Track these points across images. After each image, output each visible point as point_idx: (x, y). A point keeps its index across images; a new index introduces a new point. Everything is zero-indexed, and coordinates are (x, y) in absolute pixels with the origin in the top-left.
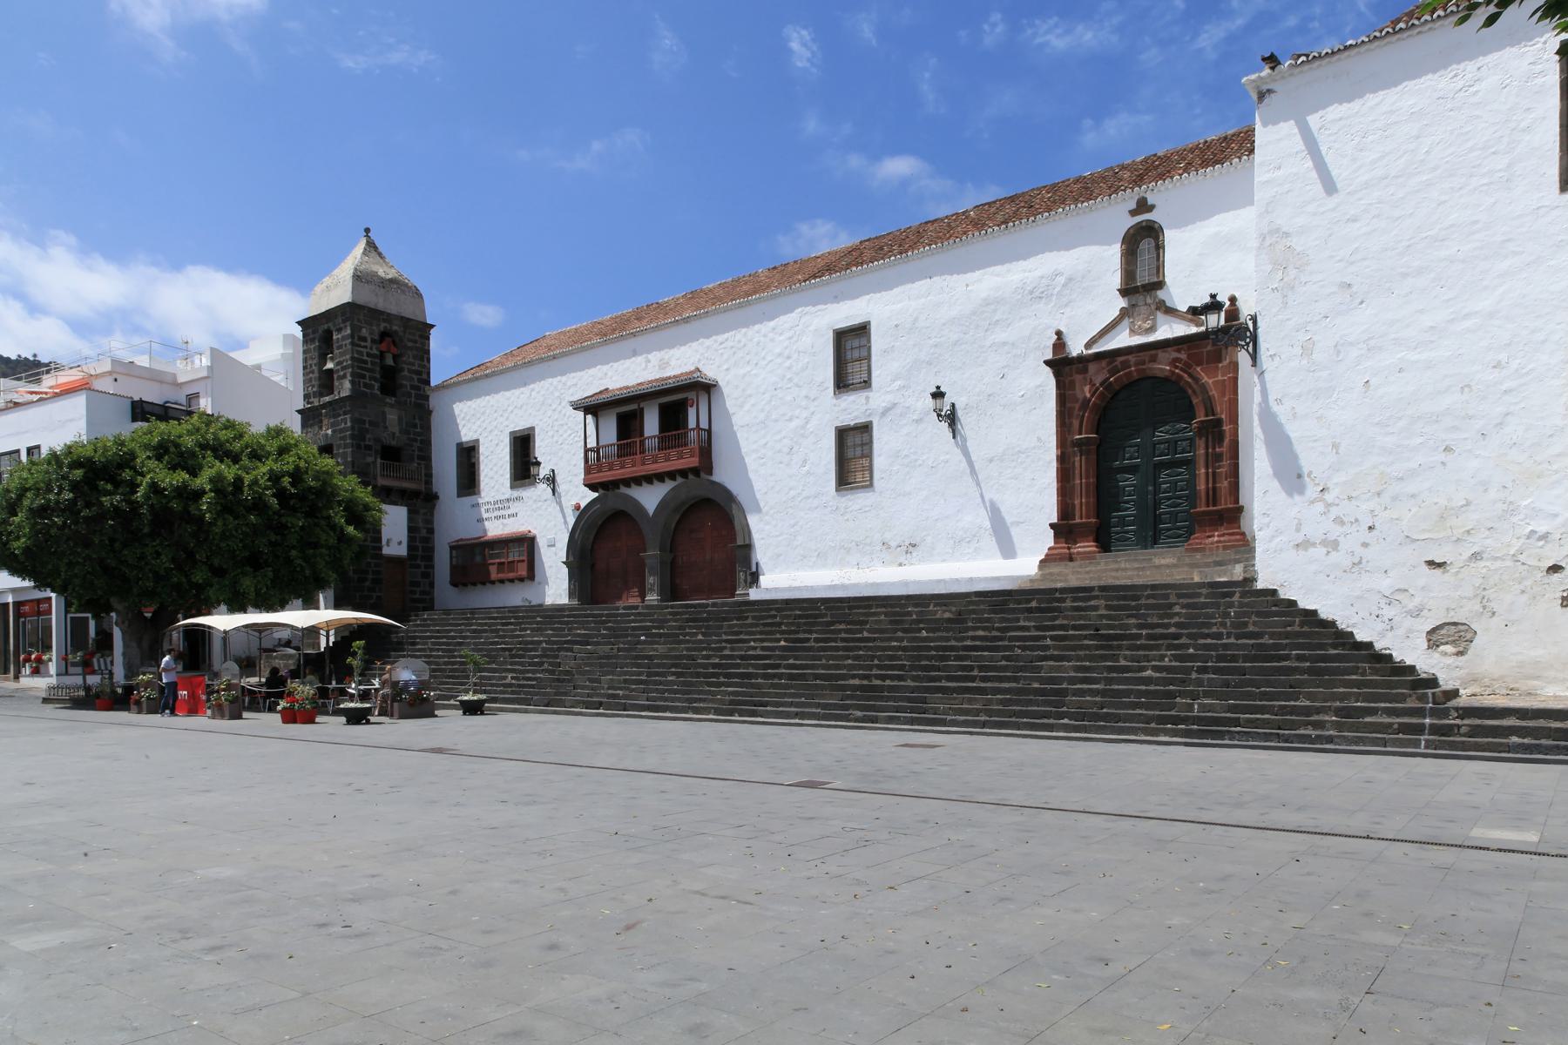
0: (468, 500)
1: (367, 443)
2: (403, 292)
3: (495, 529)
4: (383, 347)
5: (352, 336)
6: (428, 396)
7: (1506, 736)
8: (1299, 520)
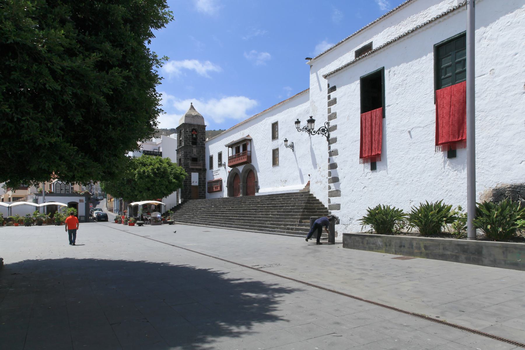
0: (211, 170)
1: (188, 157)
2: (198, 118)
3: (216, 178)
4: (193, 133)
5: (184, 131)
6: (205, 144)
7: (299, 231)
8: (316, 176)
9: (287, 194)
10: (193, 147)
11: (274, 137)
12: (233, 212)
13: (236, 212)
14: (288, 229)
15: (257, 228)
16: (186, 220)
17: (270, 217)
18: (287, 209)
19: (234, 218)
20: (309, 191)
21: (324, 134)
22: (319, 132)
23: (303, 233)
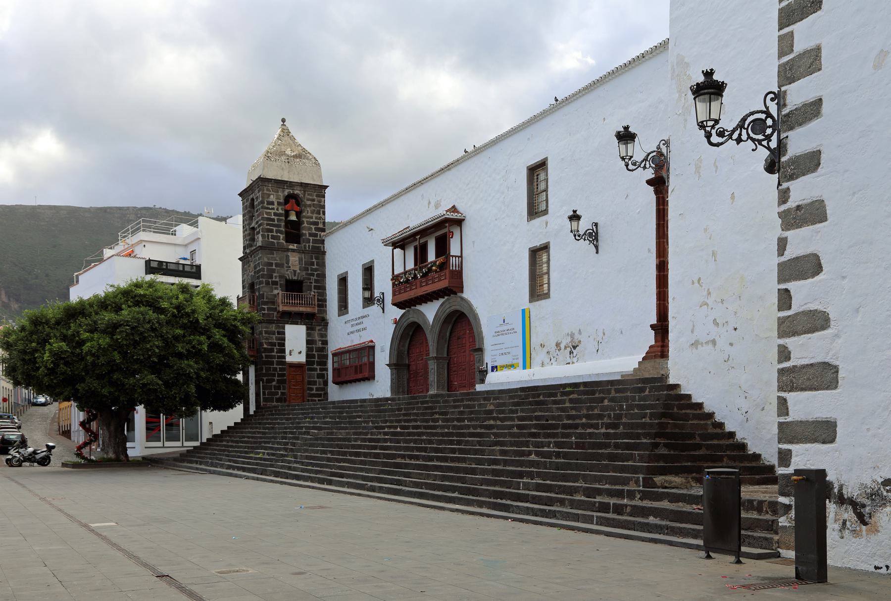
1: (274, 280)
4: (288, 207)
9: (585, 384)
10: (288, 250)
11: (535, 210)
12: (406, 441)
13: (415, 441)
14: (604, 508)
15: (487, 499)
16: (261, 465)
17: (532, 464)
18: (591, 435)
19: (408, 461)
20: (665, 377)
21: (760, 142)
22: (740, 135)
23: (667, 527)
